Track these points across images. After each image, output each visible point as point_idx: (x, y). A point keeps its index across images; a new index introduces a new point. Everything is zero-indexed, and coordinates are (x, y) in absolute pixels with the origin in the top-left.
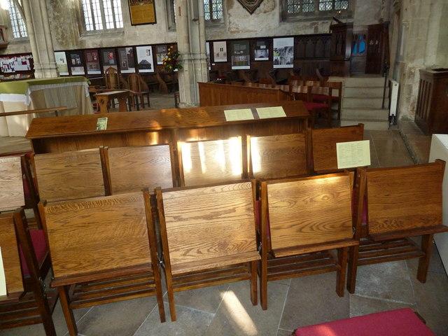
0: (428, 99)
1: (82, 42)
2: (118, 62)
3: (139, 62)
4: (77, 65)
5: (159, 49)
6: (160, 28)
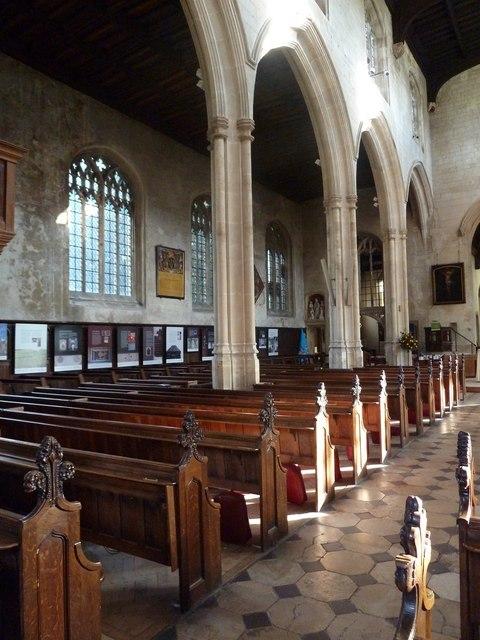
0: (228, 259)
1: (76, 310)
2: (140, 349)
3: (167, 349)
4: (69, 352)
5: (192, 333)
6: (187, 306)
